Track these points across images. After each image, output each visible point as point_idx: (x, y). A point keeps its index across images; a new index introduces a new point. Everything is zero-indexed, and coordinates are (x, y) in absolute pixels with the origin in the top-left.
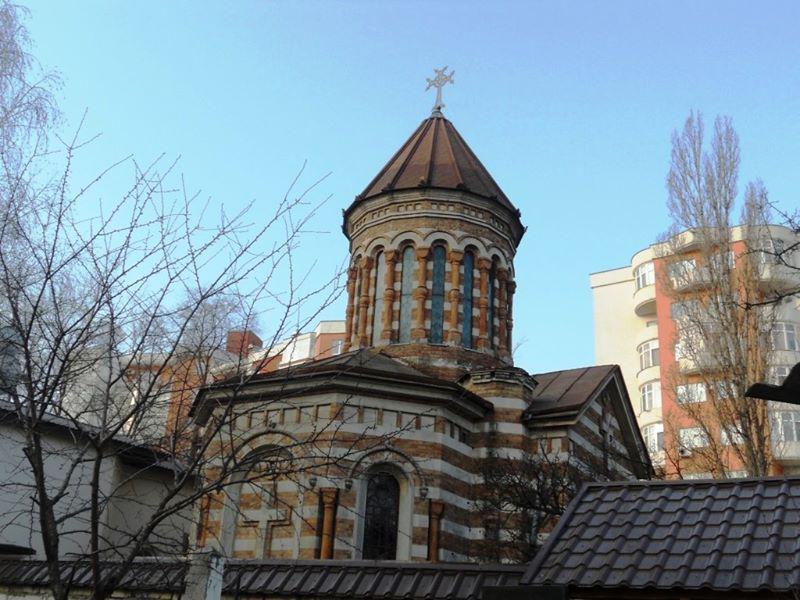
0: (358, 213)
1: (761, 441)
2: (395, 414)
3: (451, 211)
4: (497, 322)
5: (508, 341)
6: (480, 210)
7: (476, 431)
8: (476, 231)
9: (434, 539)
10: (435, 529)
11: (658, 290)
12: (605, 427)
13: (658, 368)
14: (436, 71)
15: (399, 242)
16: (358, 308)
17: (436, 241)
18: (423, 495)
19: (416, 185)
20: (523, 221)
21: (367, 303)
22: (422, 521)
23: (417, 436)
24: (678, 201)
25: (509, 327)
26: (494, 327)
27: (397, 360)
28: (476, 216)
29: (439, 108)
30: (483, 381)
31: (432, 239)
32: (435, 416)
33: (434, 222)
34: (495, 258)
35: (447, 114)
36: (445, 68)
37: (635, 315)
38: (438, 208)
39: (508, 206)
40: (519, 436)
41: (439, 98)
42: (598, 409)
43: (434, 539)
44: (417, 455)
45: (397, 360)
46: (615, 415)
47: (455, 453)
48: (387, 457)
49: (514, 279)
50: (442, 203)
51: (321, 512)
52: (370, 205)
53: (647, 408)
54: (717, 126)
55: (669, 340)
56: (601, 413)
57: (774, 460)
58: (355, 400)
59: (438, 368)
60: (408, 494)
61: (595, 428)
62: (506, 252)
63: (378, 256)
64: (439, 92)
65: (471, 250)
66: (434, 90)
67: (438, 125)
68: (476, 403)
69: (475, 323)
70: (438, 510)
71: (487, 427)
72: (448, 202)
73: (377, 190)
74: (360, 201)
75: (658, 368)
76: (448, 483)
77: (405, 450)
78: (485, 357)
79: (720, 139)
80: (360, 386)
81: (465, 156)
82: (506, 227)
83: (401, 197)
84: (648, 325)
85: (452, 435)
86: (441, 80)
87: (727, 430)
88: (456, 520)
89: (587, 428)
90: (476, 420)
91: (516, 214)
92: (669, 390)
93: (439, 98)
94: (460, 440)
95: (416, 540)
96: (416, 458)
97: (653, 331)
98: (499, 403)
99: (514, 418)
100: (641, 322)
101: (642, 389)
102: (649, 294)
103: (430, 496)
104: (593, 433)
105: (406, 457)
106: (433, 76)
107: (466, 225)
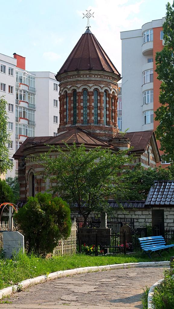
13: (152, 83)
15: (82, 89)
29: (88, 28)
35: (93, 31)
37: (142, 55)
46: (151, 146)
53: (146, 103)
64: (88, 21)
67: (87, 36)
72: (98, 74)
75: (152, 83)
80: (160, 209)
82: (116, 80)
86: (88, 16)
100: (145, 59)
106: (86, 13)
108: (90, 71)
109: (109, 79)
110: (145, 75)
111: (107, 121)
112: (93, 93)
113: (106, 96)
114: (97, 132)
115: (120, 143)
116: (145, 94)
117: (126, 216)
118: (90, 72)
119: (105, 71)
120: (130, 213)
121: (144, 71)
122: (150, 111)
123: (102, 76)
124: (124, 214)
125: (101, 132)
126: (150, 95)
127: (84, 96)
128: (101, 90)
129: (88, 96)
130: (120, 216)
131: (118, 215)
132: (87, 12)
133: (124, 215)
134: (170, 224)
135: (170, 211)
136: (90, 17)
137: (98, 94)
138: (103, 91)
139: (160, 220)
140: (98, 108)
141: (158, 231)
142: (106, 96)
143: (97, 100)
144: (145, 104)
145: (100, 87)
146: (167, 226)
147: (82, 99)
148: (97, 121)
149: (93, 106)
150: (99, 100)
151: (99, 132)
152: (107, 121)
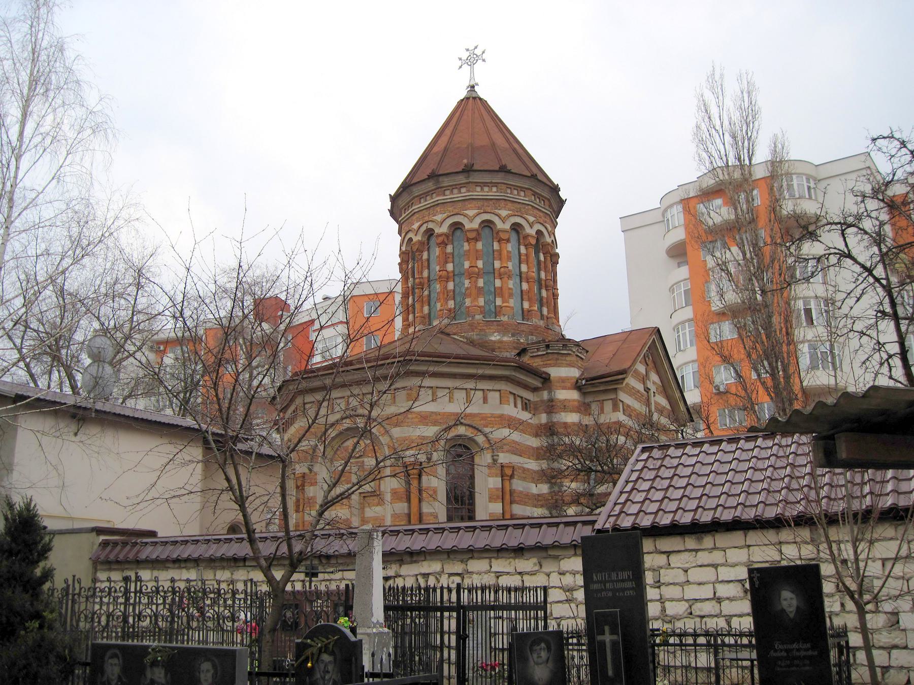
0: (405, 198)
1: (787, 377)
2: (465, 391)
3: (493, 193)
4: (544, 293)
5: (555, 310)
6: (522, 189)
7: (536, 399)
8: (520, 209)
9: (507, 497)
10: (507, 488)
11: (688, 232)
12: (650, 385)
14: (467, 50)
16: (413, 288)
17: (483, 222)
18: (495, 461)
19: (460, 170)
20: (562, 194)
21: (421, 285)
22: (495, 482)
23: (486, 410)
24: (704, 155)
25: (555, 296)
26: (541, 299)
27: (456, 337)
28: (518, 194)
29: (473, 87)
30: (540, 353)
31: (478, 220)
32: (500, 391)
33: (480, 203)
34: (539, 233)
35: (481, 92)
36: (476, 47)
38: (482, 190)
39: (545, 180)
40: (574, 400)
41: (472, 77)
42: (641, 368)
43: (507, 497)
44: (487, 427)
45: (456, 337)
46: (658, 373)
47: (521, 422)
48: (461, 430)
49: (557, 251)
50: (485, 184)
51: (408, 483)
52: (417, 191)
53: (682, 348)
54: (740, 79)
55: (700, 277)
56: (644, 373)
57: (804, 391)
58: (428, 382)
59: (495, 342)
60: (483, 460)
61: (640, 387)
62: (548, 226)
63: (428, 239)
64: (472, 72)
65: (516, 228)
66: (466, 68)
68: (535, 375)
69: (525, 297)
70: (508, 472)
71: (545, 395)
72: (491, 183)
73: (422, 175)
74: (405, 187)
76: (518, 449)
77: (477, 423)
78: (536, 327)
79: (742, 93)
81: (510, 144)
82: (546, 201)
83: (446, 182)
84: (679, 265)
85: (515, 406)
86: (472, 59)
87: (756, 370)
88: (524, 479)
89: (633, 388)
90: (535, 390)
91: (555, 189)
92: (702, 335)
93: (472, 77)
94: (523, 410)
95: (492, 499)
96: (487, 430)
97: (683, 272)
98: (556, 372)
99: (569, 385)
100: (673, 263)
101: (676, 329)
102: (679, 235)
103: (500, 461)
104: (638, 391)
105: (477, 429)
106: (465, 55)
107: (510, 204)
108: (466, 174)
109: (525, 196)
110: (675, 294)
111: (522, 309)
112: (479, 234)
113: (519, 242)
114: (493, 338)
115: (551, 357)
116: (678, 332)
117: (529, 581)
118: (469, 177)
119: (509, 172)
120: (541, 566)
121: (673, 286)
122: (691, 365)
123: (504, 187)
124: (520, 573)
125: (505, 339)
126: (687, 330)
127: (456, 244)
128: (500, 225)
129: (466, 244)
130: (504, 581)
131: (498, 577)
132: (468, 54)
133: (519, 577)
134: (698, 605)
135: (697, 551)
136: (475, 56)
137: (495, 235)
138: (507, 226)
139: (624, 590)
140: (497, 273)
141: (614, 644)
142: (519, 242)
143: (491, 252)
144: (680, 350)
145: (497, 218)
146: (691, 614)
147: (449, 254)
148: (493, 310)
149: (479, 269)
150: (497, 251)
151: (498, 338)
152: (522, 309)
